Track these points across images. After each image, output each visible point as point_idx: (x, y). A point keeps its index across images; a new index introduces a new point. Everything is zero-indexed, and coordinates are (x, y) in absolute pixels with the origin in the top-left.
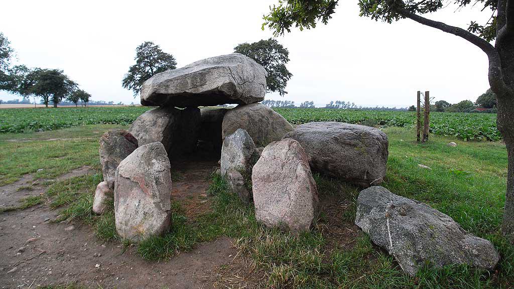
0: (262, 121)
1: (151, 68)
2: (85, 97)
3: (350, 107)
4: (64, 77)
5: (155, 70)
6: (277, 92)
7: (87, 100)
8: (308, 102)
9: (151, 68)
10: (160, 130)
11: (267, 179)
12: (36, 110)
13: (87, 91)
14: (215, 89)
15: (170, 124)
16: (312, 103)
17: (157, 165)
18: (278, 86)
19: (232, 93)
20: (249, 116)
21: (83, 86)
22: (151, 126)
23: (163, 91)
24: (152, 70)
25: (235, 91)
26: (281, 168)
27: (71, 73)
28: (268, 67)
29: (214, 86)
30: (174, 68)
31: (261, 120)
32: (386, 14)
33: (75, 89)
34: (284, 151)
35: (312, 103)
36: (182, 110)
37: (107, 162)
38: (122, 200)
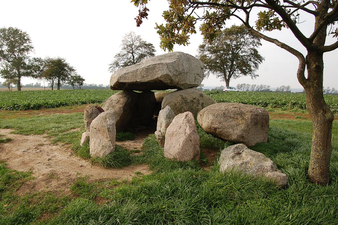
0: (193, 101)
1: (133, 55)
2: (79, 80)
3: (330, 92)
4: (66, 65)
5: (136, 56)
6: (248, 76)
7: (82, 84)
8: (284, 86)
9: (133, 55)
10: (121, 106)
11: (172, 135)
12: (45, 92)
13: (83, 76)
14: (156, 79)
15: (128, 102)
16: (288, 87)
17: (109, 122)
18: (250, 70)
19: (169, 82)
20: (183, 98)
21: (80, 72)
22: (115, 102)
23: (121, 81)
24: (134, 57)
25: (172, 80)
26: (179, 128)
27: (70, 61)
28: (240, 52)
29: (156, 77)
30: (153, 55)
31: (192, 101)
32: (265, 27)
33: (73, 74)
34: (183, 119)
35: (288, 87)
36: (138, 93)
37: (88, 122)
38: (92, 139)
